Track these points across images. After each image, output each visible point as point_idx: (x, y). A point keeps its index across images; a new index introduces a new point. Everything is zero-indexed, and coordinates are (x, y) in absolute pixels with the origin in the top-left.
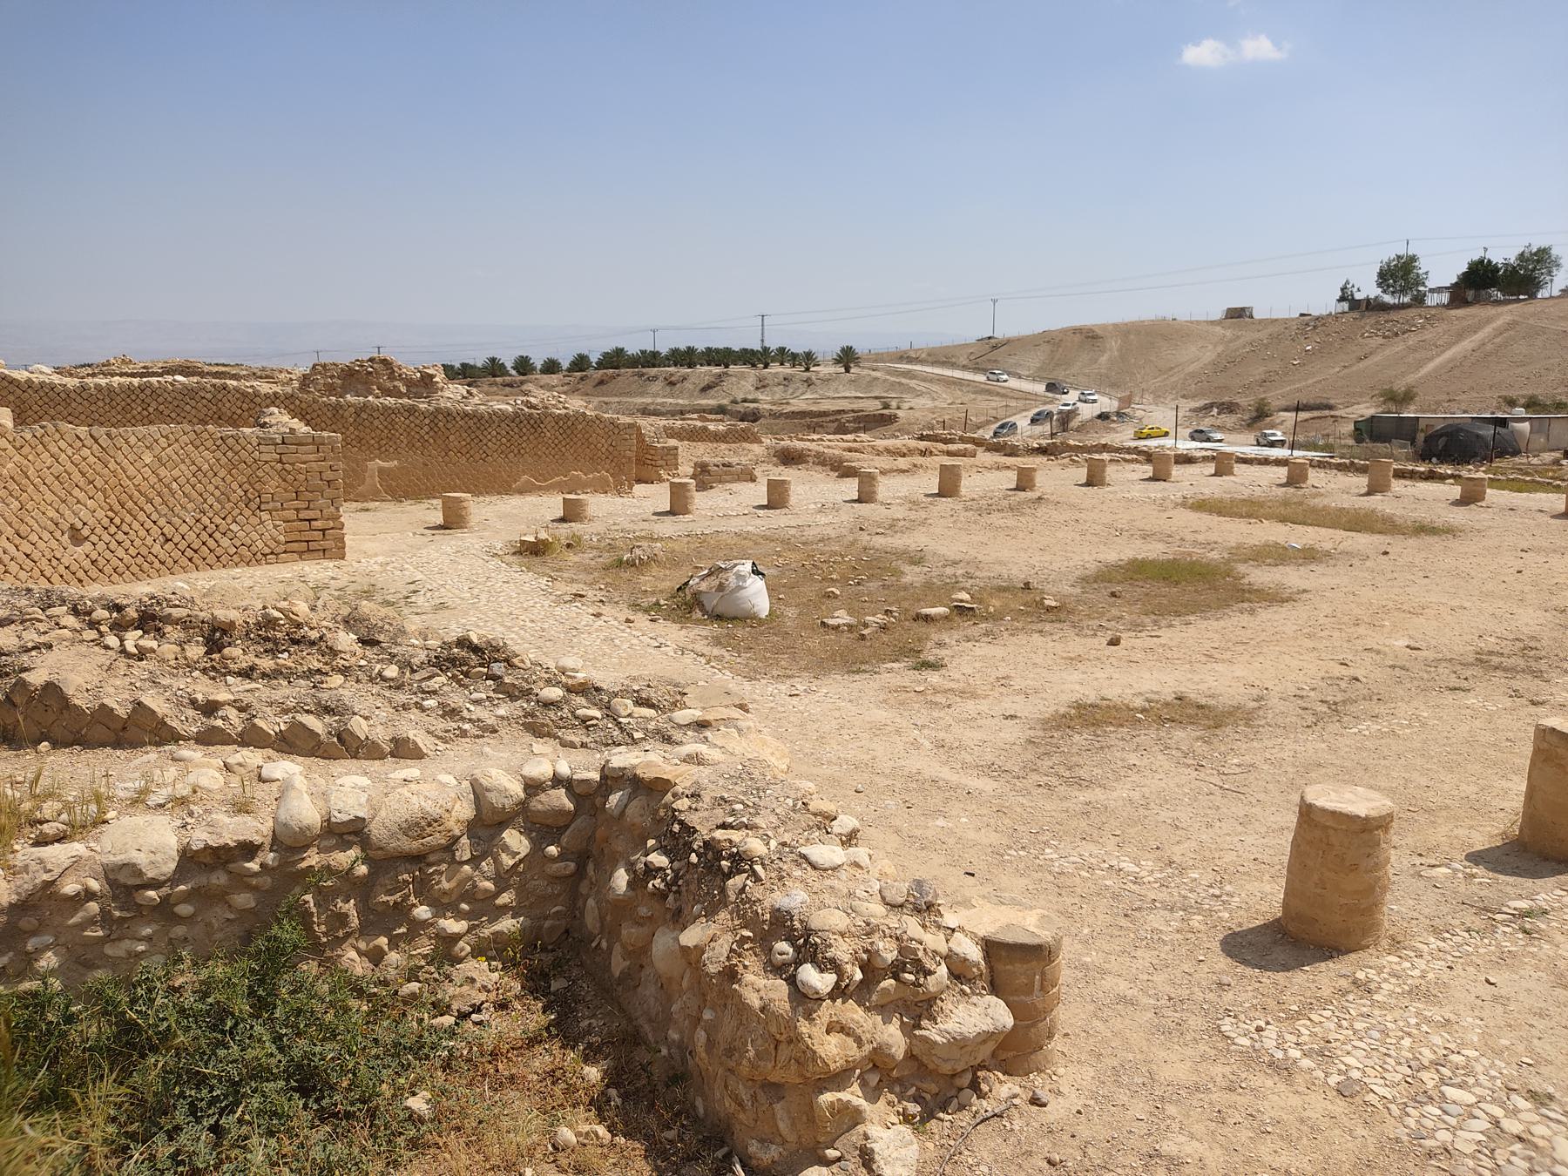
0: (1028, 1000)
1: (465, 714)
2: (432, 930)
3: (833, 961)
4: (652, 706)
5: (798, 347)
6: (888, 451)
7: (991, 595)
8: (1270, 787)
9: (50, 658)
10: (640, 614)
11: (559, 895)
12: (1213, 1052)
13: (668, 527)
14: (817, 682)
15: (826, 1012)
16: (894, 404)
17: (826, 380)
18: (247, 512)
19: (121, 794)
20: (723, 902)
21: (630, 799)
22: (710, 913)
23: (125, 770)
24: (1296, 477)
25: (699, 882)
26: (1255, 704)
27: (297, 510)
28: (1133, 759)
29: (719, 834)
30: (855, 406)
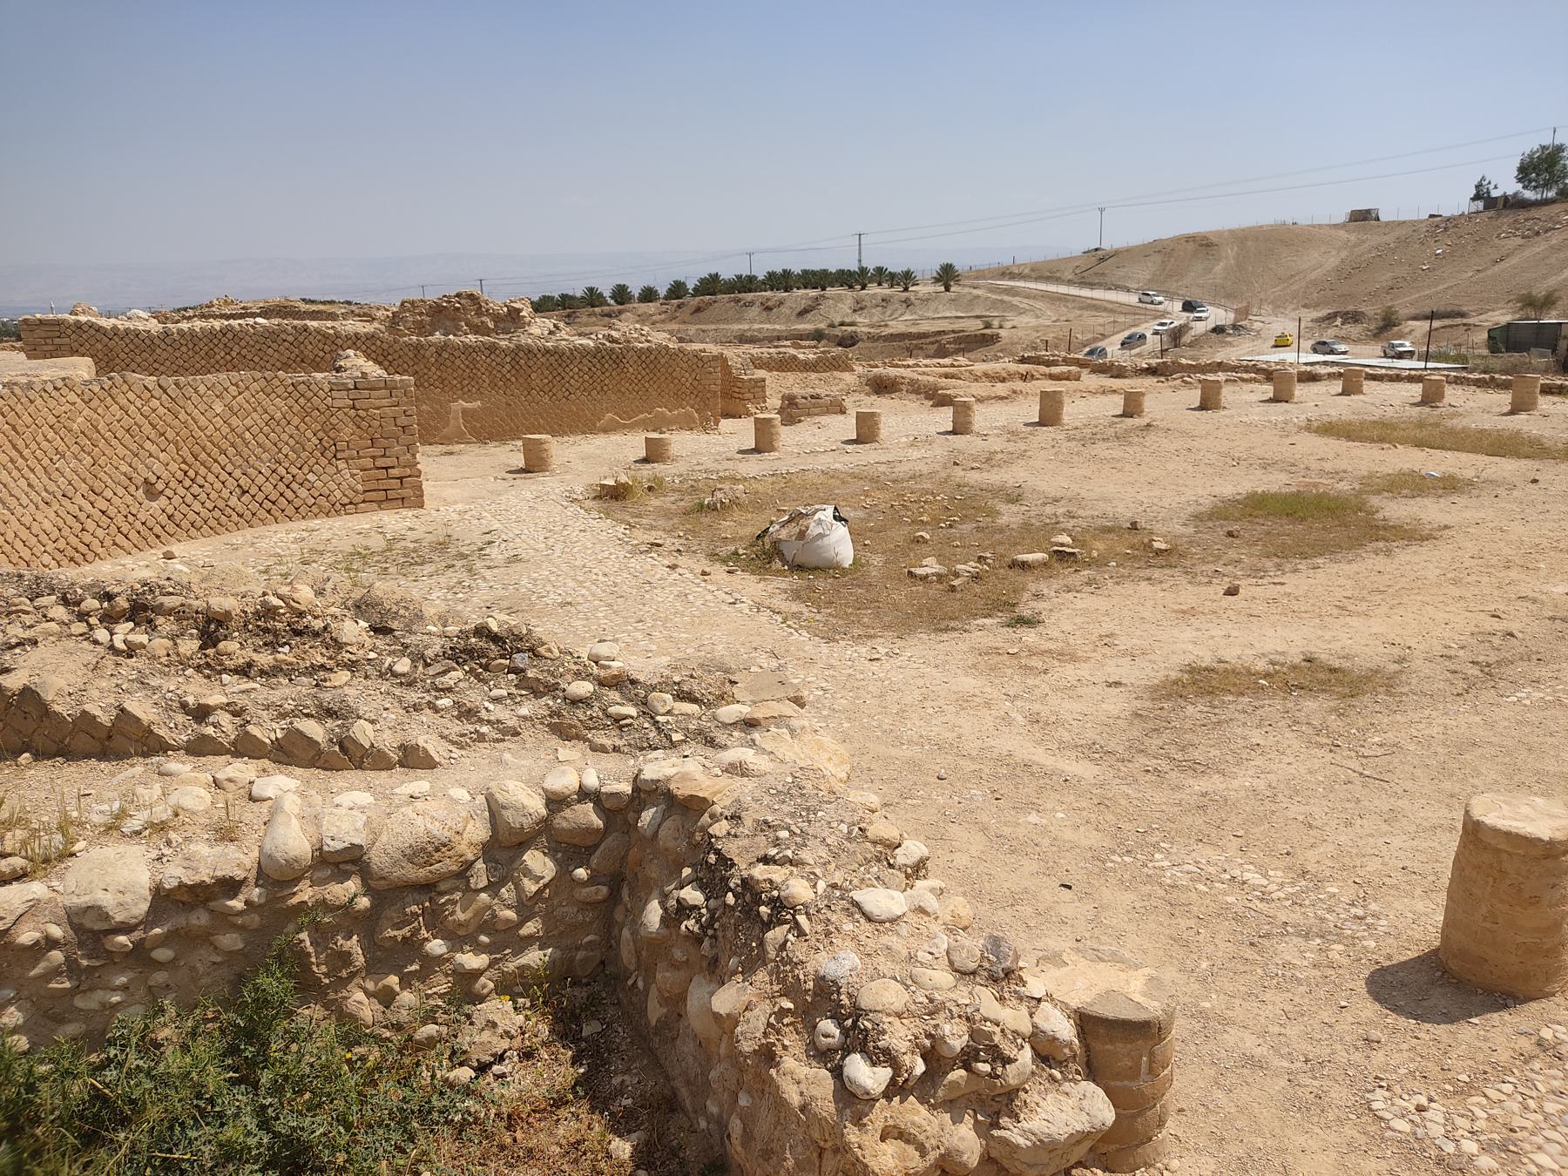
0: (1133, 1085)
1: (483, 714)
2: (448, 967)
3: (886, 1052)
4: (695, 701)
5: (895, 267)
6: (986, 375)
7: (1094, 537)
8: (1418, 772)
9: (34, 656)
10: (718, 565)
11: (591, 923)
12: (1363, 1139)
13: (753, 467)
14: (900, 643)
15: (880, 1115)
16: (996, 323)
17: (926, 300)
18: (323, 461)
19: (96, 819)
20: (762, 959)
21: (664, 819)
22: (748, 970)
23: (95, 787)
24: (1431, 397)
25: (736, 930)
26: (1396, 667)
27: (373, 458)
28: (1256, 737)
29: (759, 872)
30: (956, 327)
